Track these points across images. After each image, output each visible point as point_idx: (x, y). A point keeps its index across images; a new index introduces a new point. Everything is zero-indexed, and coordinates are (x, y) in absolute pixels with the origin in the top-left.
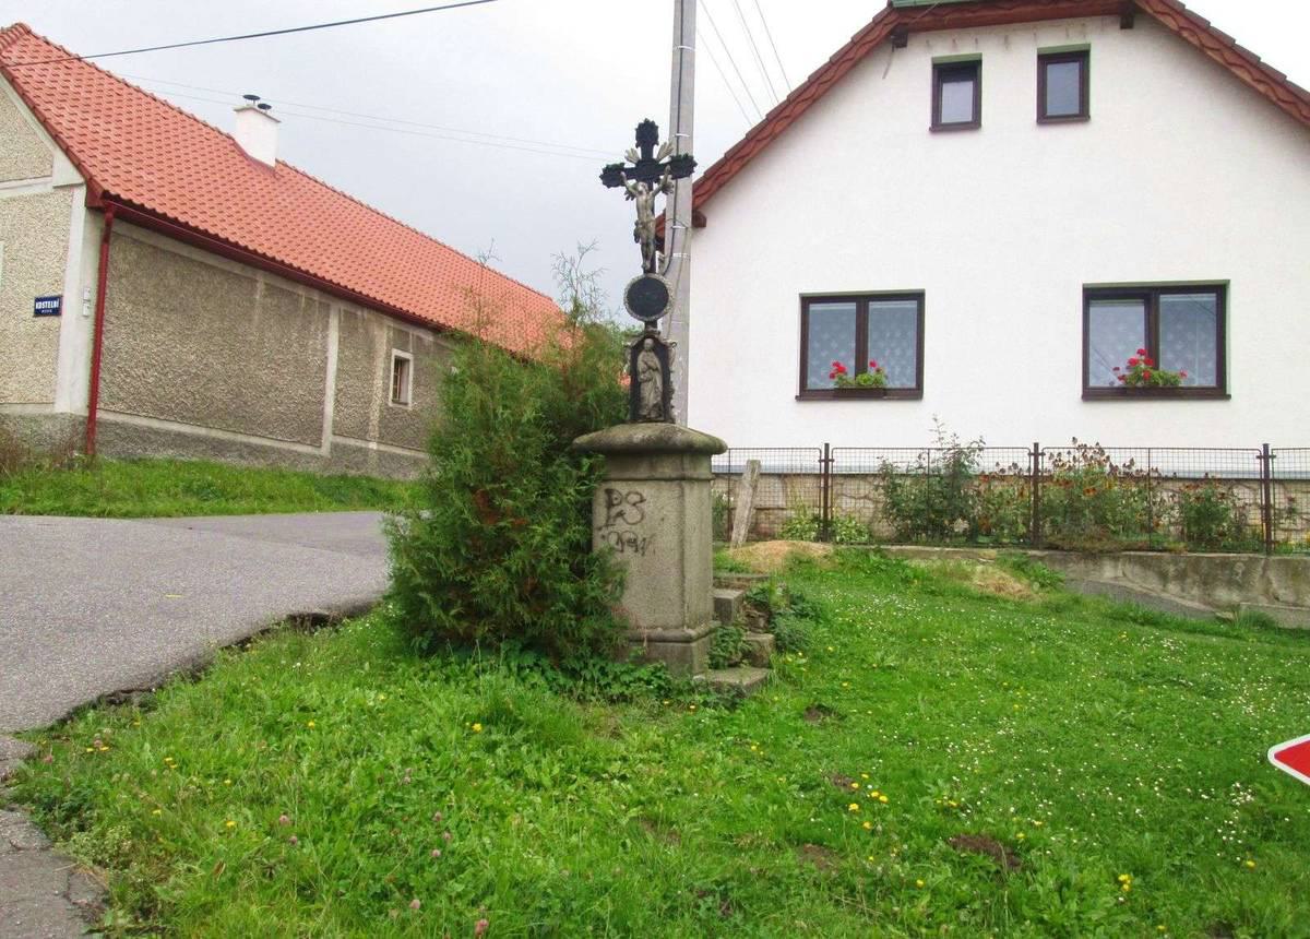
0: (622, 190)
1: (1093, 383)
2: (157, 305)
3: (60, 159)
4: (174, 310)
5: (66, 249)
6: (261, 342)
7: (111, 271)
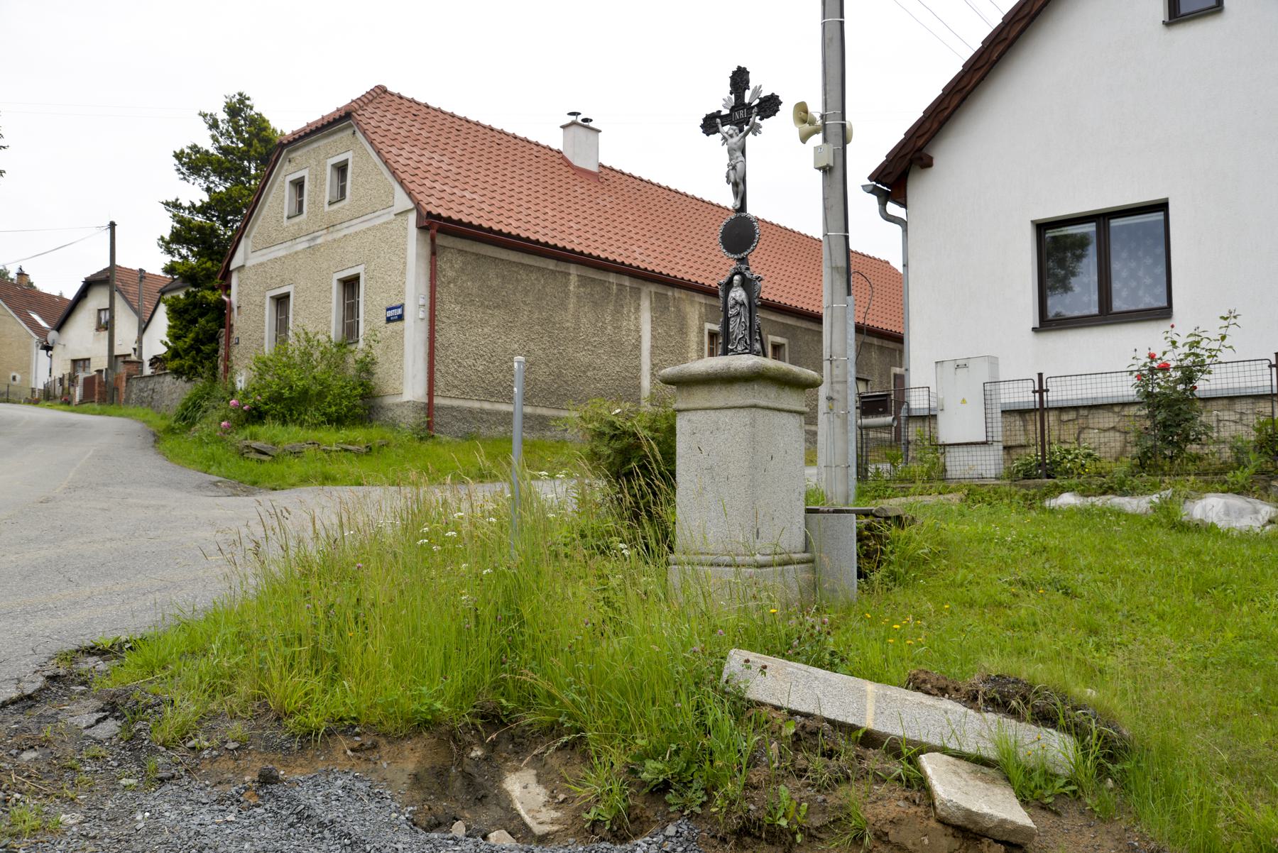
0: (718, 136)
2: (482, 304)
3: (399, 192)
4: (498, 307)
5: (405, 263)
6: (577, 328)
7: (441, 279)
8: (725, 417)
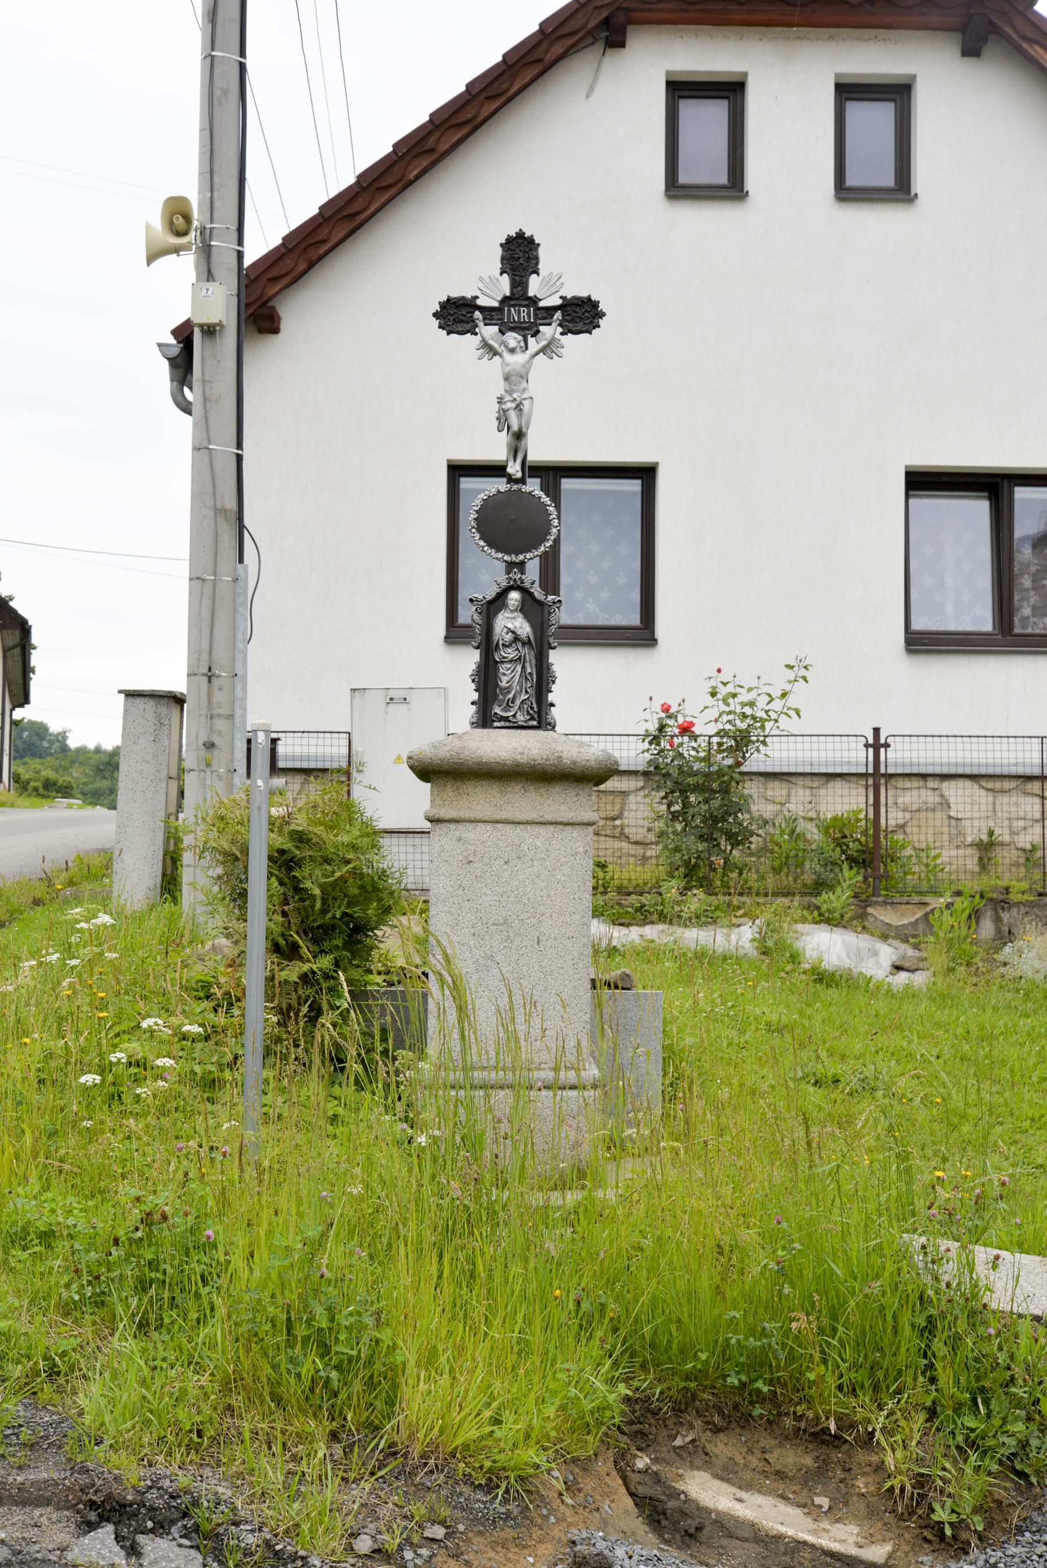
0: (470, 341)
1: (916, 626)
8: (530, 837)
